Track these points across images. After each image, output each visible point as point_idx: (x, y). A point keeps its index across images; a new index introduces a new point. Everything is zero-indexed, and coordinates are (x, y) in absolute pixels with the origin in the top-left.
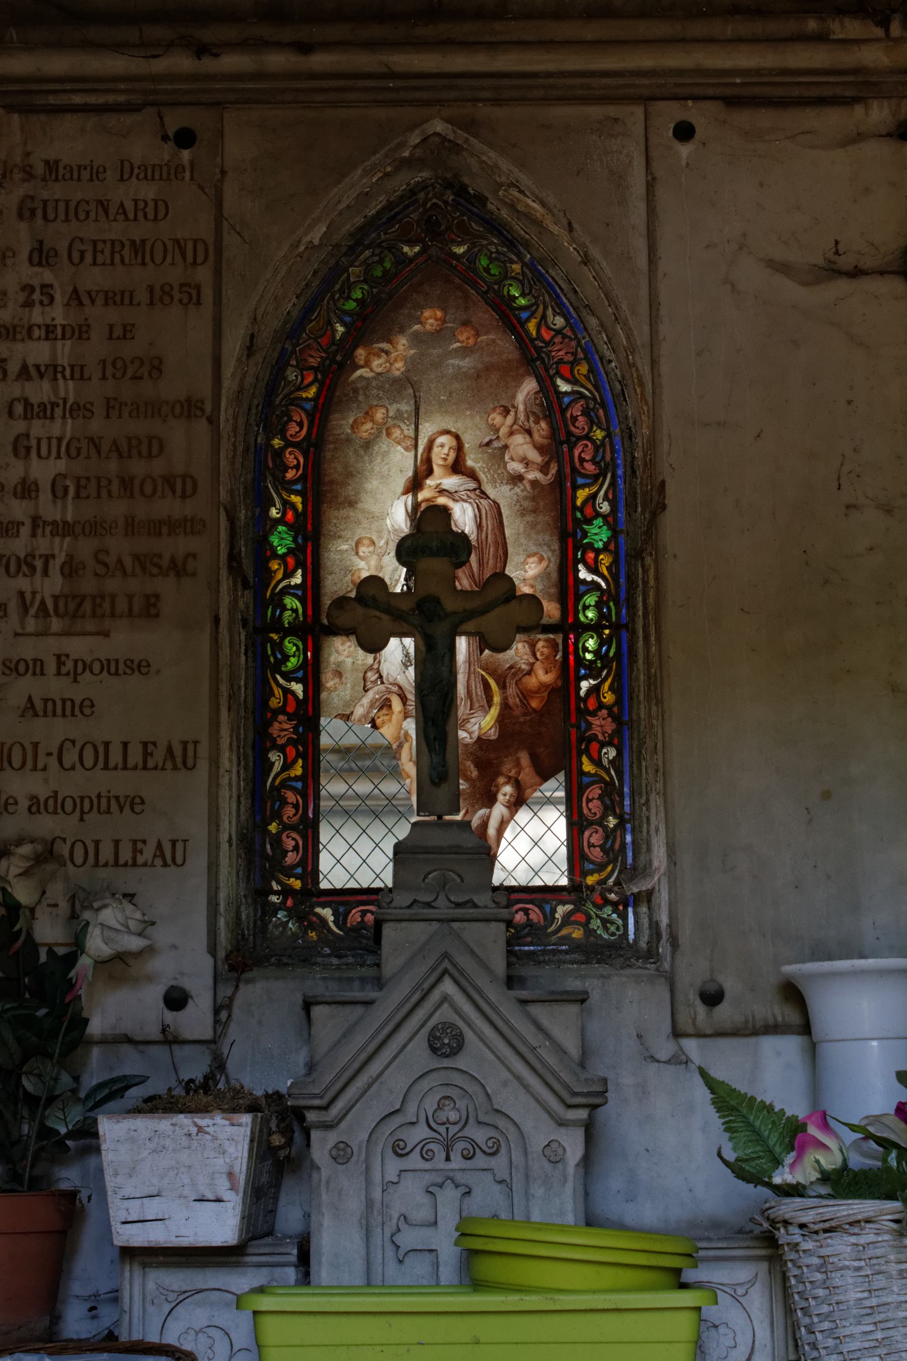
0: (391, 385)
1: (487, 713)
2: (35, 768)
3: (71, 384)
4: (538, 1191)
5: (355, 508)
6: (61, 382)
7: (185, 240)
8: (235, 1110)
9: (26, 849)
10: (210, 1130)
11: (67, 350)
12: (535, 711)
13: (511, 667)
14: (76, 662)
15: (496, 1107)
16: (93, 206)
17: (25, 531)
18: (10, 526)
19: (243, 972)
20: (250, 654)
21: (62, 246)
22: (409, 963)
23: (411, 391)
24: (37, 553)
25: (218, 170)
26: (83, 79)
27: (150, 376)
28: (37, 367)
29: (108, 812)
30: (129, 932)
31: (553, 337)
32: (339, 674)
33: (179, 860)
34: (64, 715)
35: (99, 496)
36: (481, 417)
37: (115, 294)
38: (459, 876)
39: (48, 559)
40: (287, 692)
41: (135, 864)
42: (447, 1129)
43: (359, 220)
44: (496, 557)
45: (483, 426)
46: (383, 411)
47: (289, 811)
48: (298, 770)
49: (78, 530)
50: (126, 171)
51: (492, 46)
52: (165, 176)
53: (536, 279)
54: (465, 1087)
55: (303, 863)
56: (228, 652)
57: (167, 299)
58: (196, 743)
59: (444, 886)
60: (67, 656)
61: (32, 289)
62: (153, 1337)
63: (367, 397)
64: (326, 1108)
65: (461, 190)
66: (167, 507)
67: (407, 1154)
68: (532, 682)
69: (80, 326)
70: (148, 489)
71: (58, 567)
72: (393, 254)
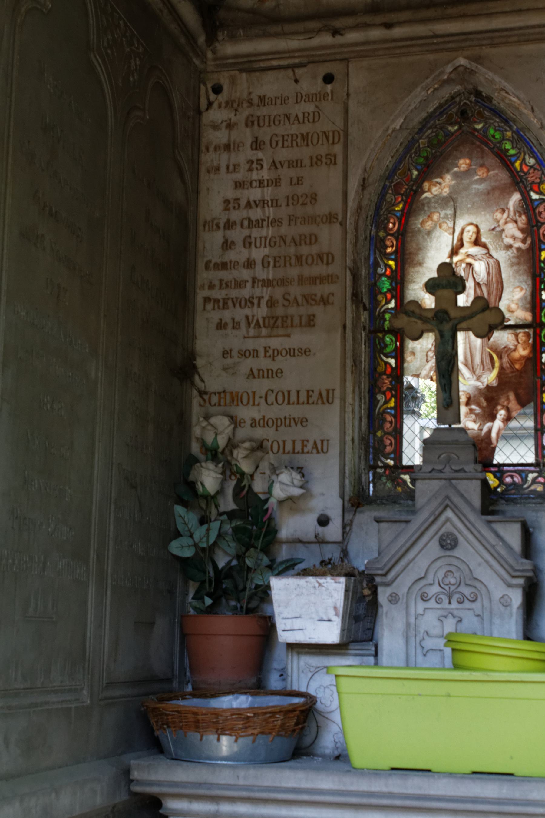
0: (442, 201)
1: (491, 372)
2: (254, 405)
3: (271, 209)
4: (497, 621)
5: (423, 266)
6: (266, 208)
7: (329, 132)
8: (339, 575)
9: (247, 445)
10: (325, 585)
11: (269, 192)
12: (517, 370)
13: (505, 348)
14: (274, 350)
15: (475, 576)
16: (282, 117)
17: (249, 285)
18: (242, 283)
19: (358, 507)
20: (367, 344)
21: (267, 139)
22: (429, 500)
23: (452, 203)
24: (255, 296)
25: (345, 94)
26: (278, 52)
27: (311, 202)
28: (255, 202)
29: (290, 426)
30: (295, 486)
31: (529, 170)
32: (413, 353)
33: (325, 450)
34: (268, 377)
35: (285, 265)
36: (490, 215)
37: (293, 162)
38: (457, 455)
39: (260, 298)
40: (387, 363)
41: (303, 452)
42: (449, 587)
43: (424, 115)
44: (497, 289)
45: (491, 219)
46: (438, 214)
47: (388, 425)
48: (392, 404)
49: (275, 283)
50: (299, 98)
51: (464, 16)
52: (318, 99)
53: (521, 139)
54: (459, 566)
55: (394, 452)
56: (352, 343)
57: (319, 163)
58: (333, 390)
59: (449, 462)
60: (270, 347)
61: (252, 162)
62: (303, 690)
63: (429, 207)
64: (385, 575)
65: (478, 94)
66: (319, 270)
67: (428, 600)
68: (516, 355)
69: (276, 179)
70: (310, 261)
71: (265, 303)
72: (443, 131)
